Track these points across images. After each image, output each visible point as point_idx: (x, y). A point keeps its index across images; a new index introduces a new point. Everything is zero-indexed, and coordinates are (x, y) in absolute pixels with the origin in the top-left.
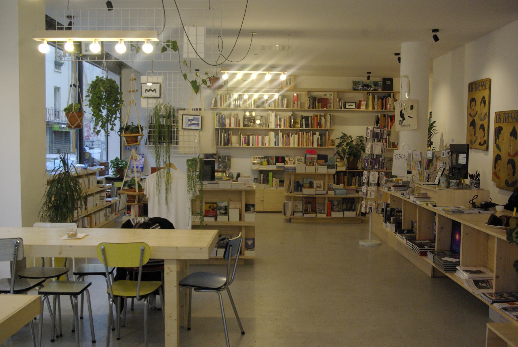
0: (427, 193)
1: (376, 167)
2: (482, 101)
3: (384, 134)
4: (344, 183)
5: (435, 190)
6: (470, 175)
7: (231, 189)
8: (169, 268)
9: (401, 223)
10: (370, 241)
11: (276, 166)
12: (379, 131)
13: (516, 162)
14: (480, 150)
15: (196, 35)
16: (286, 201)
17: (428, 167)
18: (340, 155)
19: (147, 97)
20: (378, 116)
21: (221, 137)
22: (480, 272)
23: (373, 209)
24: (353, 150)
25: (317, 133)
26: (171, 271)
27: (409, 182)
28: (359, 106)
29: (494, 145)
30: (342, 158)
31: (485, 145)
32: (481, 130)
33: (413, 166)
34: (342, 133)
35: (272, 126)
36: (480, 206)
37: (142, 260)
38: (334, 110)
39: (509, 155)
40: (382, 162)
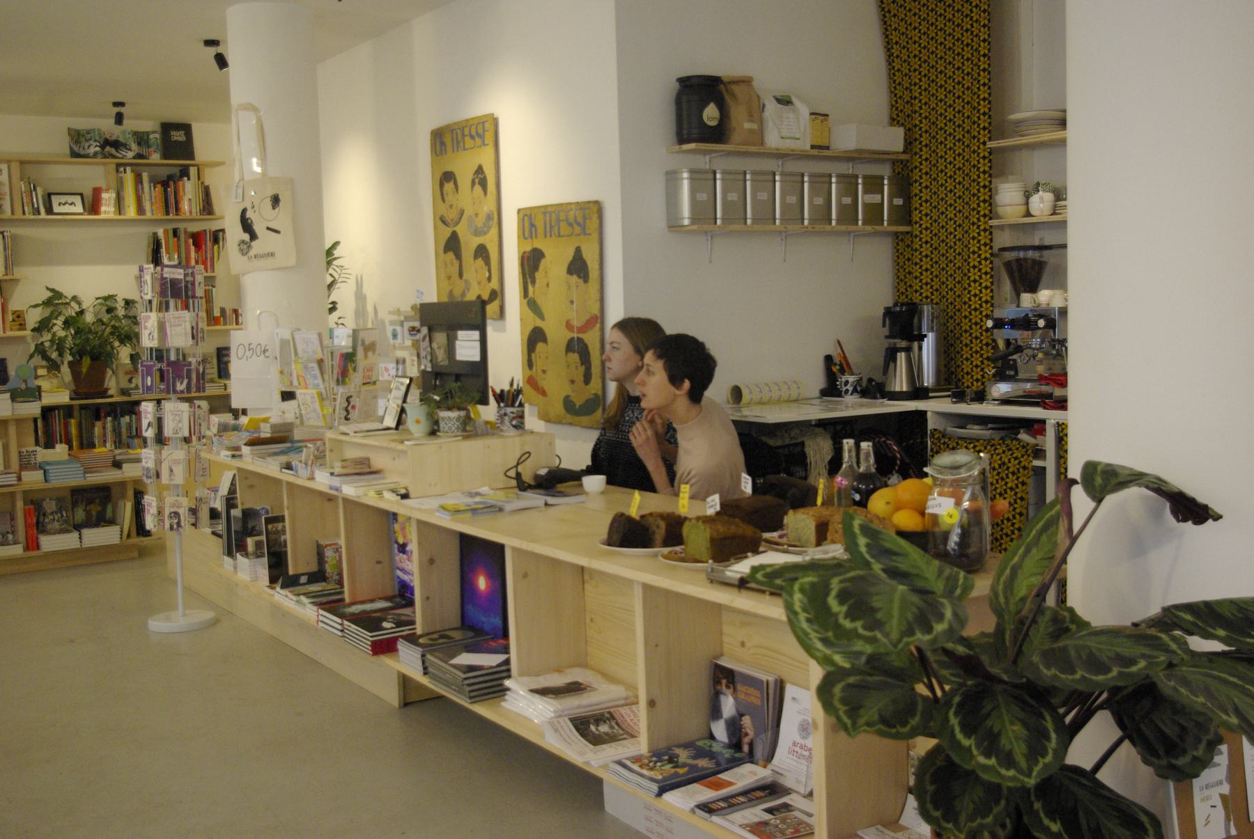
0: (368, 459)
1: (181, 387)
2: (477, 181)
3: (197, 284)
4: (68, 442)
5: (400, 447)
9: (286, 553)
12: (182, 277)
17: (343, 377)
18: (45, 356)
20: (155, 234)
22: (574, 688)
23: (182, 518)
24: (88, 340)
27: (291, 424)
28: (93, 206)
30: (54, 367)
32: (480, 262)
33: (298, 376)
34: (48, 289)
36: (532, 483)
38: (15, 217)
39: (569, 326)
40: (198, 371)
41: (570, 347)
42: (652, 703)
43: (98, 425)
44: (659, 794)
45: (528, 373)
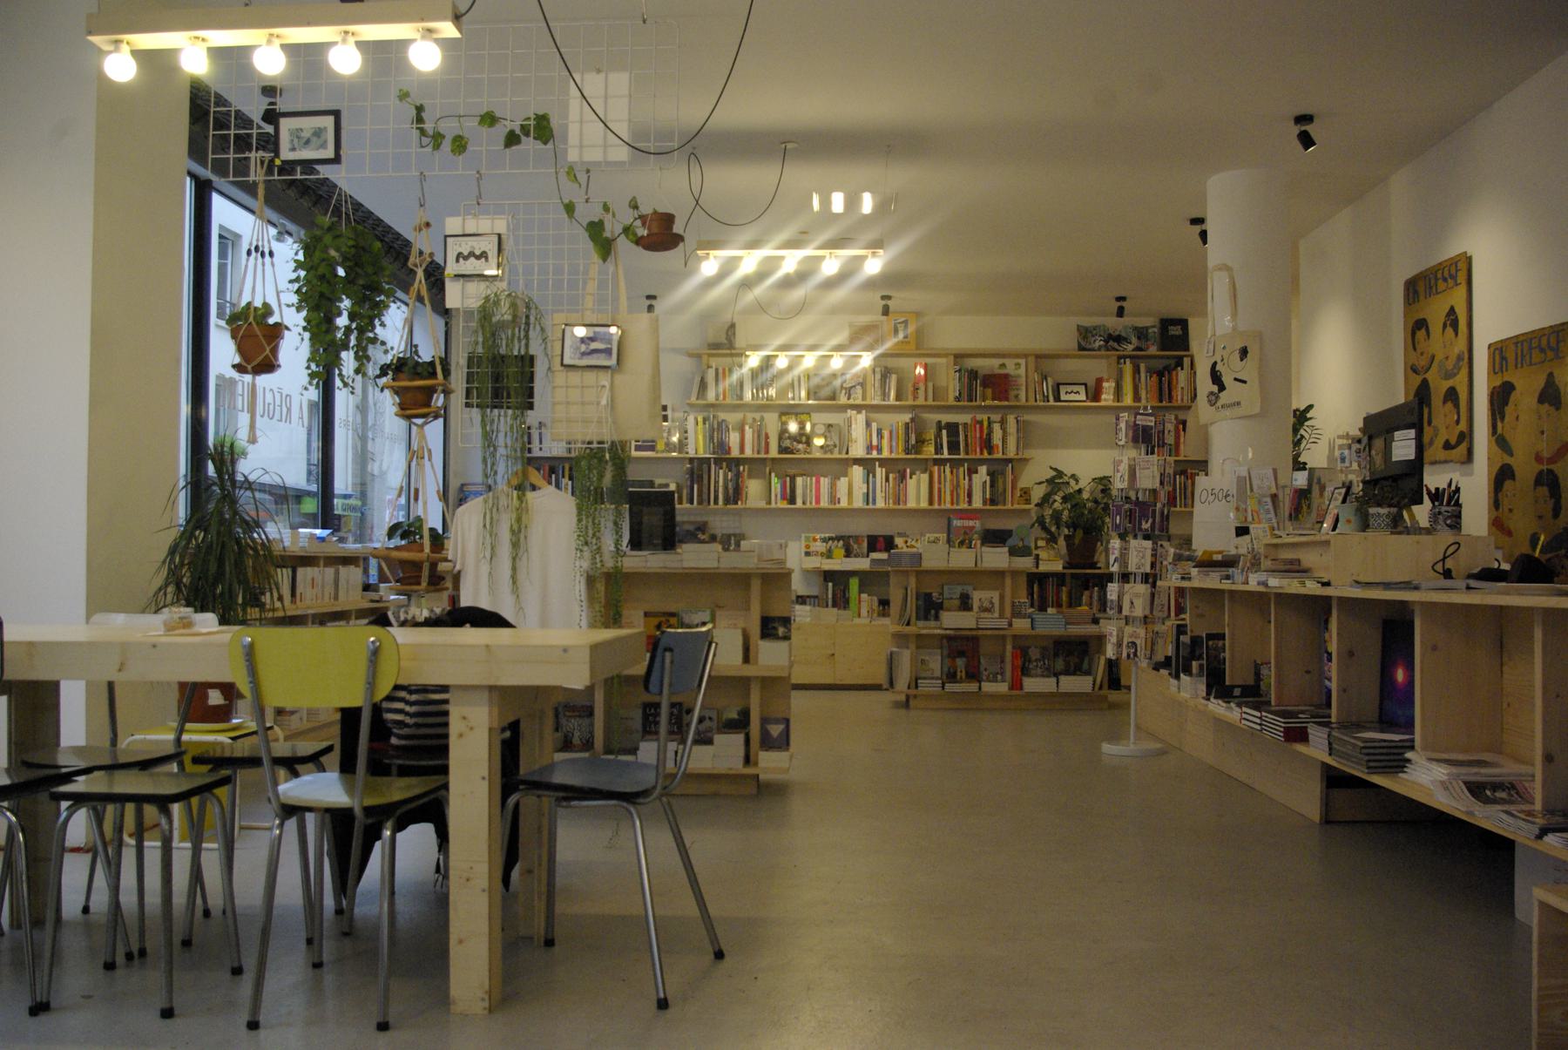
1: (1146, 526)
3: (1166, 432)
6: (1429, 493)
7: (717, 568)
8: (464, 718)
10: (1134, 743)
11: (869, 559)
12: (1153, 424)
13: (1560, 476)
14: (1447, 466)
15: (606, 97)
16: (895, 649)
18: (1044, 528)
19: (463, 276)
21: (717, 482)
23: (1139, 649)
25: (983, 470)
26: (471, 729)
28: (1095, 395)
29: (1489, 441)
30: (1052, 539)
31: (1463, 447)
32: (1449, 405)
34: (1051, 468)
35: (858, 451)
37: (371, 684)
38: (1029, 404)
39: (1538, 459)
40: (1162, 513)
41: (1538, 481)
42: (1548, 758)
43: (1086, 593)
44: (1540, 837)
45: (1495, 514)
